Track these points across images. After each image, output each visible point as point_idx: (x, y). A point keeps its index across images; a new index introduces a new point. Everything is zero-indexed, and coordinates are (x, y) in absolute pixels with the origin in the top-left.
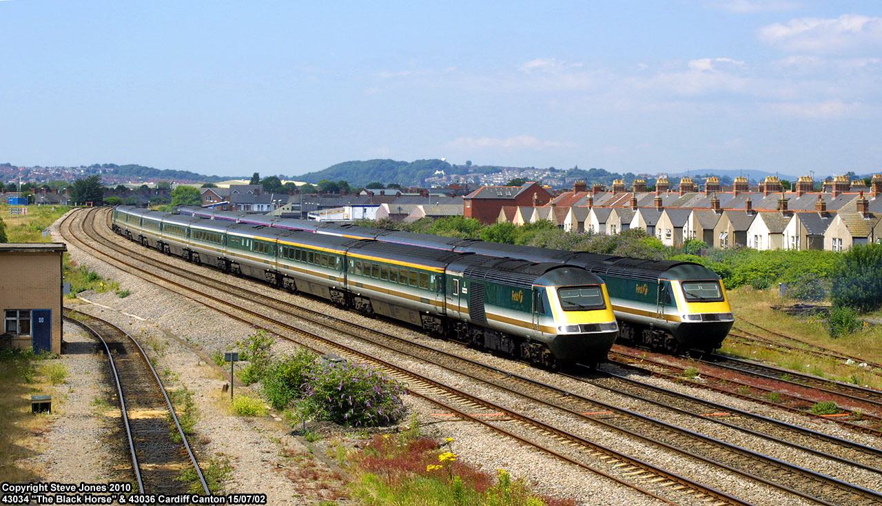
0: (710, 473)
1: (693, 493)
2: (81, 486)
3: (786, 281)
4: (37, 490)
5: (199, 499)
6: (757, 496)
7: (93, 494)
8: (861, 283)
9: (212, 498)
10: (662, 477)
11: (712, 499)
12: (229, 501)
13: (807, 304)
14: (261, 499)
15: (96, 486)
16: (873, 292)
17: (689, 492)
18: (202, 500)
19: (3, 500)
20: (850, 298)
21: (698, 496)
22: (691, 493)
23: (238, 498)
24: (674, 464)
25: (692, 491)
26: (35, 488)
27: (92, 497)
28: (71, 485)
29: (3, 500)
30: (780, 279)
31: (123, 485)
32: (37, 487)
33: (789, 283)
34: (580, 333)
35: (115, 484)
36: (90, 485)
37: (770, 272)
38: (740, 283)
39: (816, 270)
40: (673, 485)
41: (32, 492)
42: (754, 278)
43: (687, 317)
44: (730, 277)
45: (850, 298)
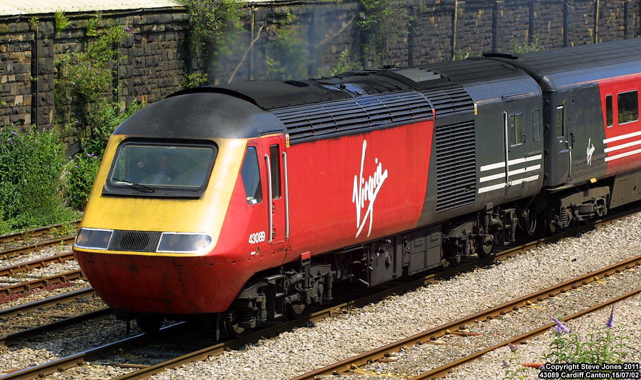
2: (603, 365)
4: (571, 368)
5: (566, 375)
9: (600, 374)
12: (613, 376)
15: (614, 365)
18: (568, 375)
26: (570, 367)
27: (602, 373)
31: (634, 365)
32: (571, 366)
35: (628, 364)
36: (609, 365)
43: (406, 260)
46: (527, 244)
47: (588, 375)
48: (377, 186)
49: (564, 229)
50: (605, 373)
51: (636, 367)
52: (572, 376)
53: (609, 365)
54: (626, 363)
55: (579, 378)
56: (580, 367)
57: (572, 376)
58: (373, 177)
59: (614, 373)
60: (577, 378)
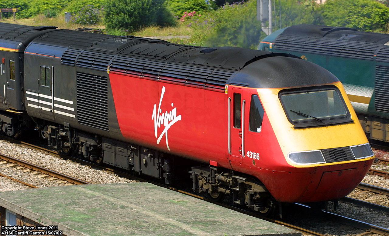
0: (33, 154)
1: (22, 169)
3: (70, 11)
4: (17, 229)
5: (17, 233)
6: (70, 169)
7: (40, 231)
8: (127, 11)
9: (38, 232)
10: (5, 161)
11: (36, 172)
13: (87, 27)
14: (60, 233)
16: (136, 17)
17: (19, 168)
19: (2, 233)
20: (119, 23)
21: (25, 171)
22: (19, 169)
23: (50, 232)
24: (5, 148)
25: (21, 167)
26: (16, 228)
27: (39, 232)
28: (32, 227)
29: (2, 233)
30: (65, 9)
32: (17, 228)
33: (72, 13)
34: (324, 164)
35: (51, 226)
37: (57, 5)
38: (35, 14)
39: (92, 3)
40: (6, 164)
41: (15, 230)
42: (46, 9)
44: (28, 9)
45: (119, 23)
46: (107, 168)
47: (31, 233)
48: (171, 121)
49: (9, 136)
50: (41, 232)
51: (56, 228)
52: (21, 233)
53: (40, 227)
54: (50, 226)
55: (36, 235)
56: (22, 228)
57: (21, 233)
58: (169, 113)
59: (46, 232)
60: (24, 235)
